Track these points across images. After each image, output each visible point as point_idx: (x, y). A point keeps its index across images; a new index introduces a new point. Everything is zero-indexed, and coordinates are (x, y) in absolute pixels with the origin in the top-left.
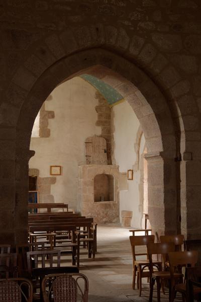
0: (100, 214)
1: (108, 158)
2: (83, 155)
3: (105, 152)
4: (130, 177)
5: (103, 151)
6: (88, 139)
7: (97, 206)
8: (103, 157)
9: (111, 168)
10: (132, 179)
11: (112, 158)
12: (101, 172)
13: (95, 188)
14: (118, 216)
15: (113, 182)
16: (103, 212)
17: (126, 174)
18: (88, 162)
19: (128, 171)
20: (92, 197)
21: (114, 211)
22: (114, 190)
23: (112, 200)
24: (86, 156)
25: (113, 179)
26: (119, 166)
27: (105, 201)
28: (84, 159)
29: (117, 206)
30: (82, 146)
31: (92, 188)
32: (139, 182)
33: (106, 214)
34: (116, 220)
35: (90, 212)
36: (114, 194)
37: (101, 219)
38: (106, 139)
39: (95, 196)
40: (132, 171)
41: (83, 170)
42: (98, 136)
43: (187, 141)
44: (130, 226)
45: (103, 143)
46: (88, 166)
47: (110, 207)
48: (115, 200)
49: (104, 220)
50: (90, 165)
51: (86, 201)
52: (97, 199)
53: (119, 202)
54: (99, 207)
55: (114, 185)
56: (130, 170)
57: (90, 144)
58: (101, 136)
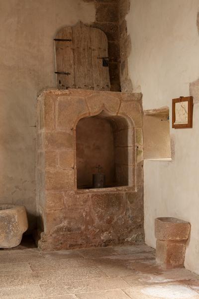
0: (92, 221)
1: (111, 80)
2: (48, 71)
3: (105, 64)
4: (182, 118)
5: (101, 61)
6: (62, 30)
7: (85, 201)
8: (101, 75)
9: (121, 100)
10: (190, 125)
11: (122, 79)
12: (95, 111)
13: (79, 153)
14: (141, 226)
15: (127, 136)
16: (101, 217)
17: (162, 115)
18: (62, 85)
19: (175, 101)
20: (70, 175)
21: (129, 213)
22: (130, 157)
23: (125, 182)
24: (55, 40)
25: (126, 128)
26: (141, 95)
27: (105, 186)
28: (52, 79)
29: (137, 199)
30: (48, 49)
31: (71, 152)
32: (132, 180)
33: (109, 222)
34: (134, 236)
35: (65, 218)
36: (130, 168)
37: (96, 235)
38: (106, 34)
39: (79, 171)
40: (190, 100)
41: (45, 105)
42: (86, 25)
43: (107, 195)
44: (182, 266)
45: (98, 44)
46: (59, 92)
47: (120, 203)
48: (130, 184)
49: (104, 237)
50: (67, 91)
51: (55, 188)
52: (85, 182)
53: (141, 189)
54: (90, 203)
55: (130, 143)
56: (181, 99)
57: (68, 43)
58: (95, 26)
